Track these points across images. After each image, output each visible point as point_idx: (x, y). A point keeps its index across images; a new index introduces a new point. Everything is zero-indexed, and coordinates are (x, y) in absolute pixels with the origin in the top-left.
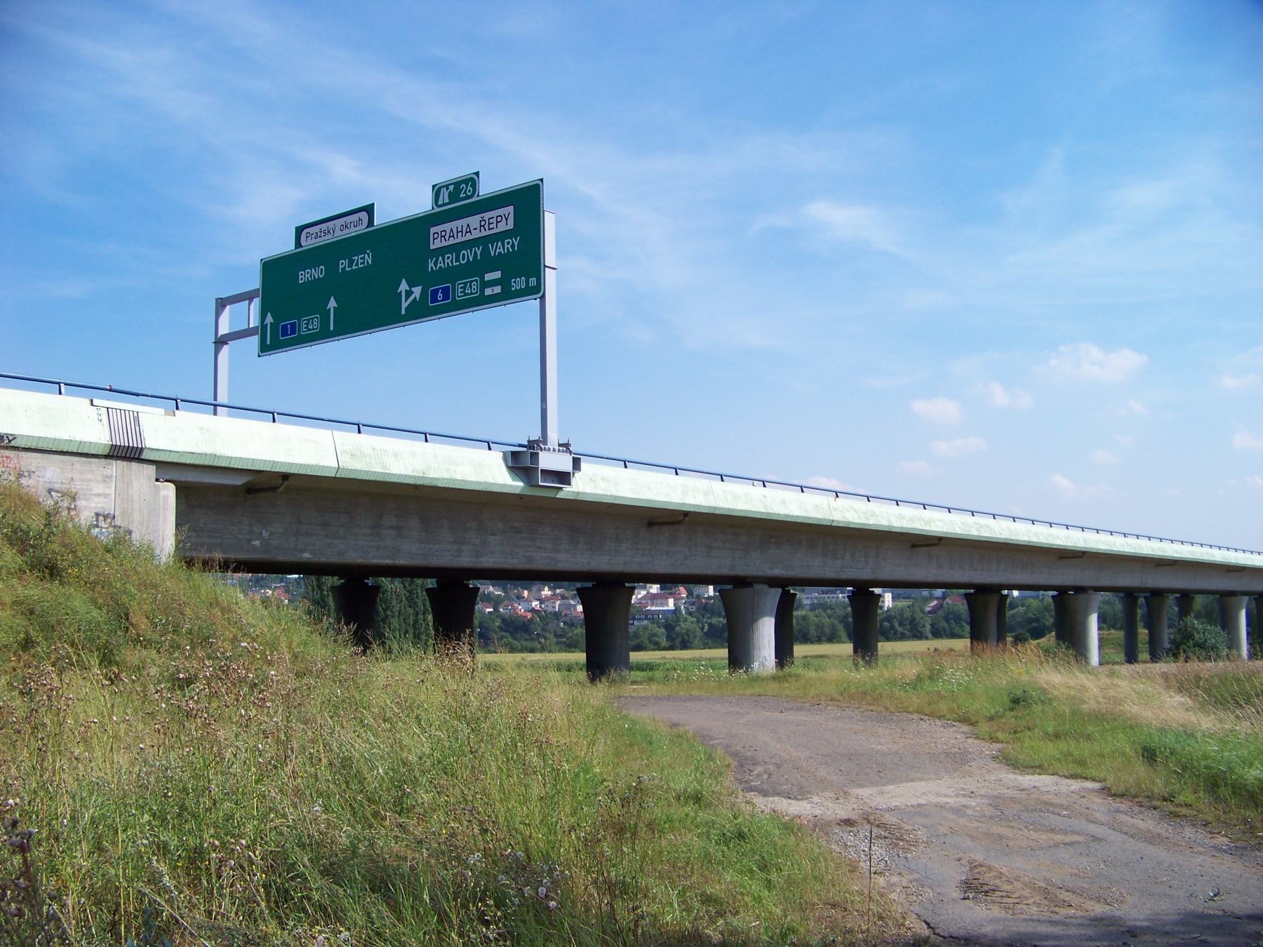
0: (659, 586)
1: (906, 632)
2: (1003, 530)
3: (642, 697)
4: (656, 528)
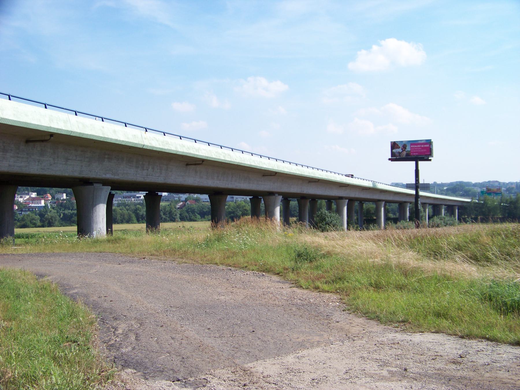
0: (36, 193)
1: (167, 218)
2: (237, 157)
3: (20, 254)
4: (31, 144)
